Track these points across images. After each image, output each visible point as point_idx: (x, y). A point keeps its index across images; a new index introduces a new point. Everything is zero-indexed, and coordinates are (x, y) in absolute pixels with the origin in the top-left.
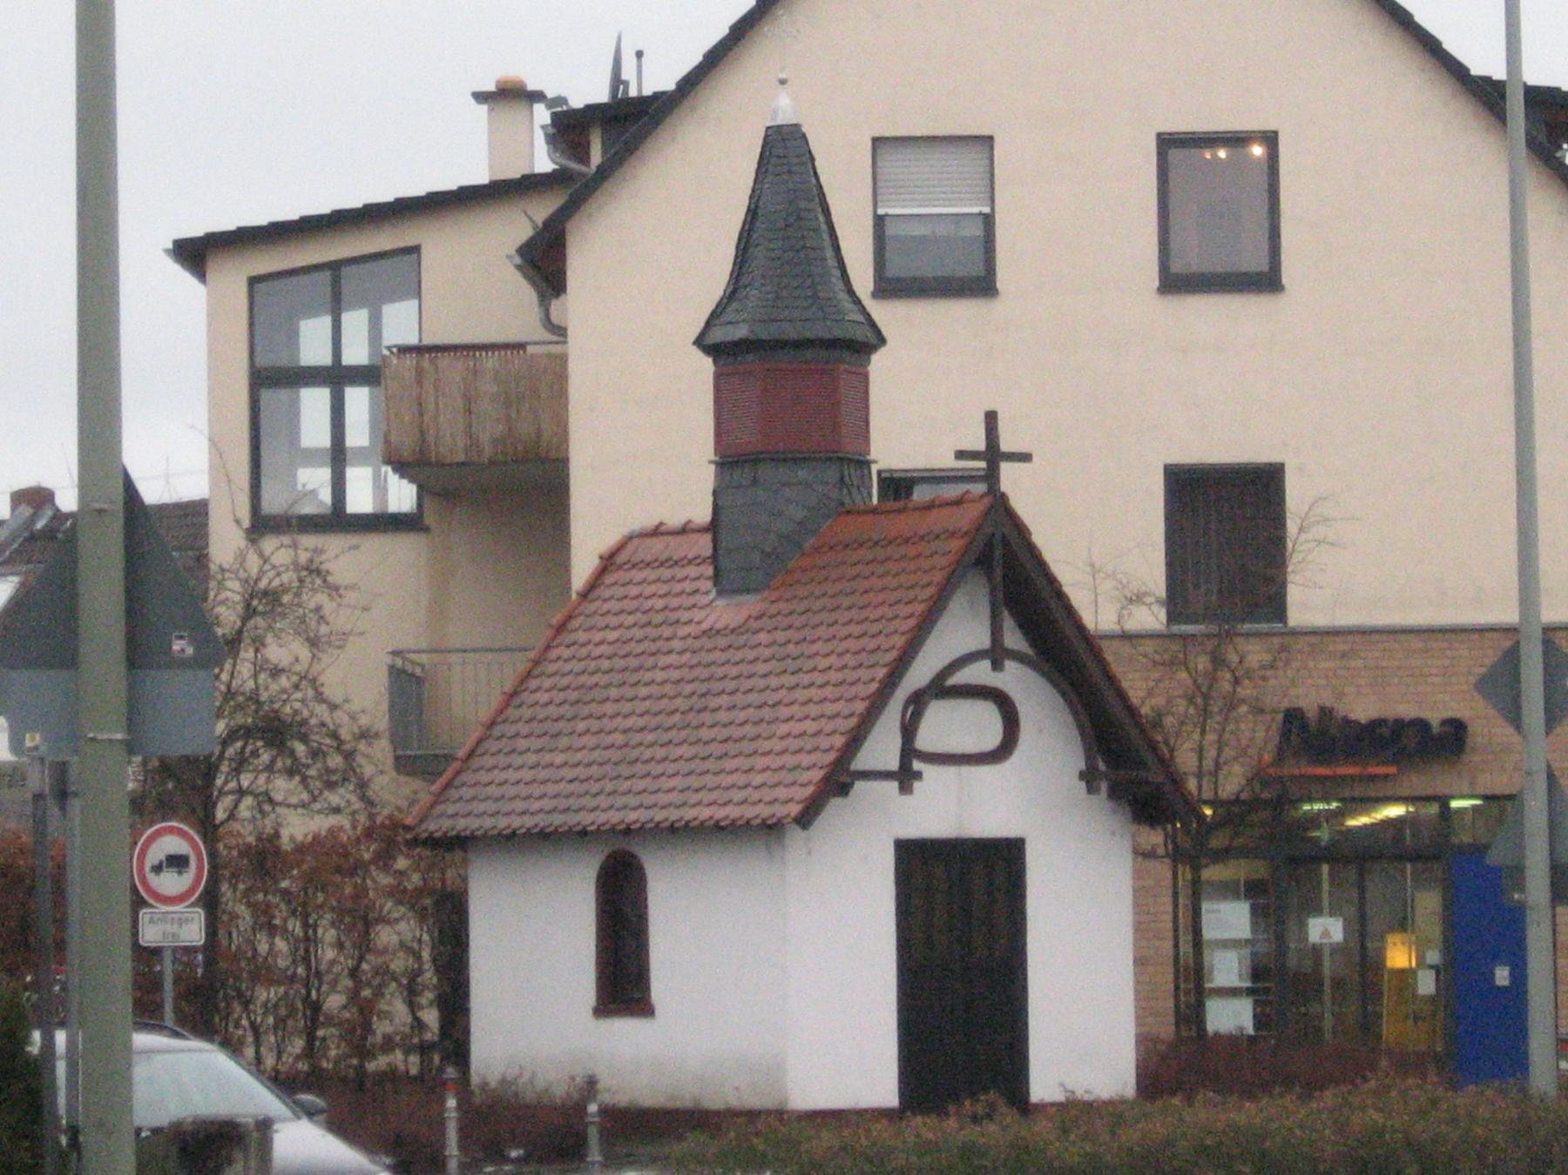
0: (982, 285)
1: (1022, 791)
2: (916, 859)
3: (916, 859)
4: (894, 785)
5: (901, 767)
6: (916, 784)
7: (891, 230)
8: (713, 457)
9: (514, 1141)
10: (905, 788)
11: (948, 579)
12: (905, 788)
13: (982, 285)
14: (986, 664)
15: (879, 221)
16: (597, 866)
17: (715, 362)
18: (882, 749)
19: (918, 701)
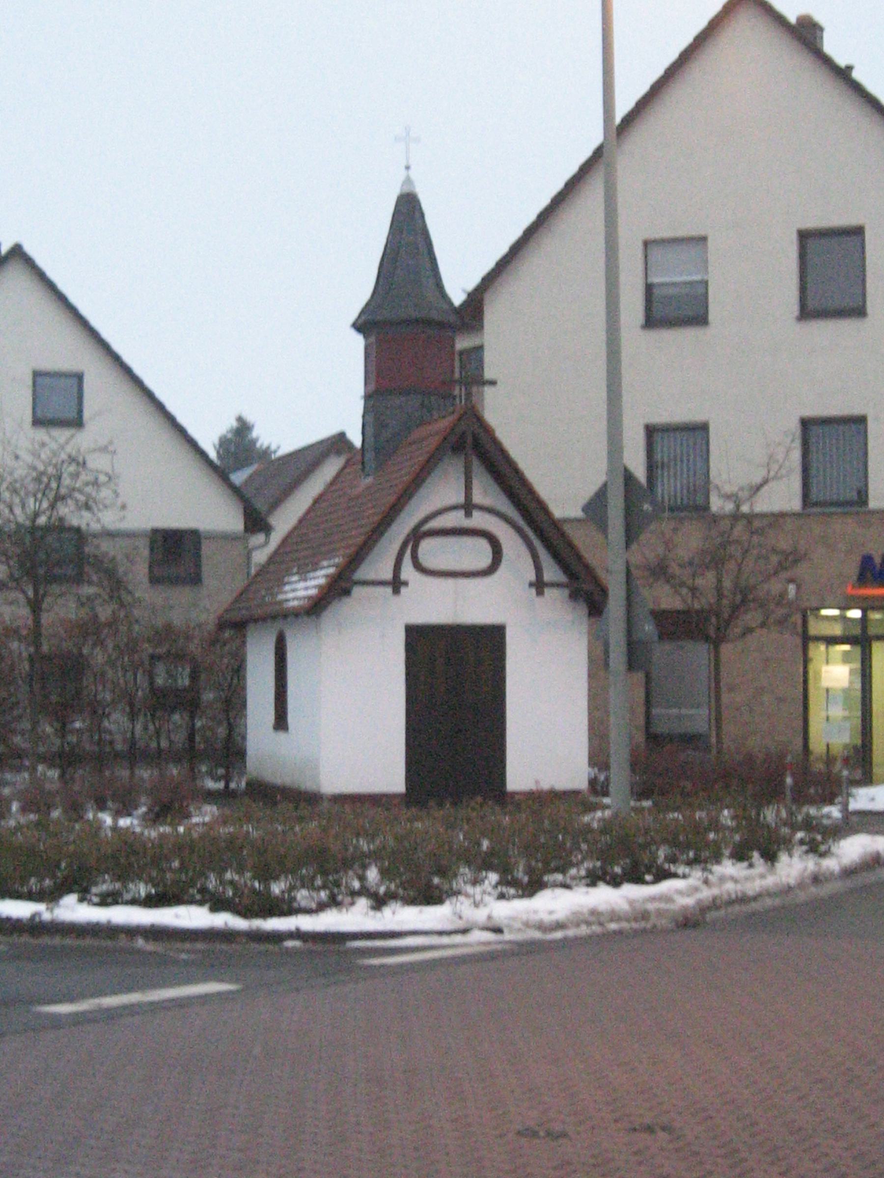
0: (700, 319)
1: (500, 596)
2: (422, 642)
3: (422, 642)
4: (389, 590)
5: (537, 580)
6: (403, 590)
7: (656, 292)
8: (488, 390)
9: (649, 872)
10: (396, 591)
11: (428, 461)
12: (396, 591)
13: (700, 319)
14: (461, 513)
15: (649, 289)
16: (274, 640)
17: (365, 337)
18: (380, 565)
19: (417, 536)
